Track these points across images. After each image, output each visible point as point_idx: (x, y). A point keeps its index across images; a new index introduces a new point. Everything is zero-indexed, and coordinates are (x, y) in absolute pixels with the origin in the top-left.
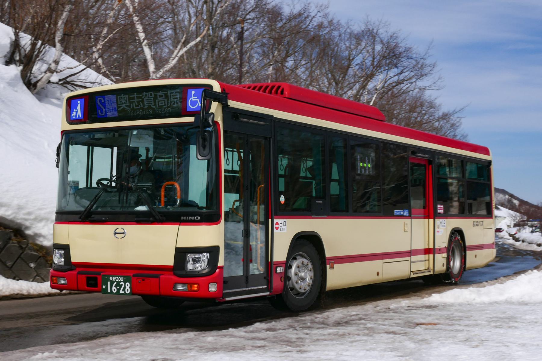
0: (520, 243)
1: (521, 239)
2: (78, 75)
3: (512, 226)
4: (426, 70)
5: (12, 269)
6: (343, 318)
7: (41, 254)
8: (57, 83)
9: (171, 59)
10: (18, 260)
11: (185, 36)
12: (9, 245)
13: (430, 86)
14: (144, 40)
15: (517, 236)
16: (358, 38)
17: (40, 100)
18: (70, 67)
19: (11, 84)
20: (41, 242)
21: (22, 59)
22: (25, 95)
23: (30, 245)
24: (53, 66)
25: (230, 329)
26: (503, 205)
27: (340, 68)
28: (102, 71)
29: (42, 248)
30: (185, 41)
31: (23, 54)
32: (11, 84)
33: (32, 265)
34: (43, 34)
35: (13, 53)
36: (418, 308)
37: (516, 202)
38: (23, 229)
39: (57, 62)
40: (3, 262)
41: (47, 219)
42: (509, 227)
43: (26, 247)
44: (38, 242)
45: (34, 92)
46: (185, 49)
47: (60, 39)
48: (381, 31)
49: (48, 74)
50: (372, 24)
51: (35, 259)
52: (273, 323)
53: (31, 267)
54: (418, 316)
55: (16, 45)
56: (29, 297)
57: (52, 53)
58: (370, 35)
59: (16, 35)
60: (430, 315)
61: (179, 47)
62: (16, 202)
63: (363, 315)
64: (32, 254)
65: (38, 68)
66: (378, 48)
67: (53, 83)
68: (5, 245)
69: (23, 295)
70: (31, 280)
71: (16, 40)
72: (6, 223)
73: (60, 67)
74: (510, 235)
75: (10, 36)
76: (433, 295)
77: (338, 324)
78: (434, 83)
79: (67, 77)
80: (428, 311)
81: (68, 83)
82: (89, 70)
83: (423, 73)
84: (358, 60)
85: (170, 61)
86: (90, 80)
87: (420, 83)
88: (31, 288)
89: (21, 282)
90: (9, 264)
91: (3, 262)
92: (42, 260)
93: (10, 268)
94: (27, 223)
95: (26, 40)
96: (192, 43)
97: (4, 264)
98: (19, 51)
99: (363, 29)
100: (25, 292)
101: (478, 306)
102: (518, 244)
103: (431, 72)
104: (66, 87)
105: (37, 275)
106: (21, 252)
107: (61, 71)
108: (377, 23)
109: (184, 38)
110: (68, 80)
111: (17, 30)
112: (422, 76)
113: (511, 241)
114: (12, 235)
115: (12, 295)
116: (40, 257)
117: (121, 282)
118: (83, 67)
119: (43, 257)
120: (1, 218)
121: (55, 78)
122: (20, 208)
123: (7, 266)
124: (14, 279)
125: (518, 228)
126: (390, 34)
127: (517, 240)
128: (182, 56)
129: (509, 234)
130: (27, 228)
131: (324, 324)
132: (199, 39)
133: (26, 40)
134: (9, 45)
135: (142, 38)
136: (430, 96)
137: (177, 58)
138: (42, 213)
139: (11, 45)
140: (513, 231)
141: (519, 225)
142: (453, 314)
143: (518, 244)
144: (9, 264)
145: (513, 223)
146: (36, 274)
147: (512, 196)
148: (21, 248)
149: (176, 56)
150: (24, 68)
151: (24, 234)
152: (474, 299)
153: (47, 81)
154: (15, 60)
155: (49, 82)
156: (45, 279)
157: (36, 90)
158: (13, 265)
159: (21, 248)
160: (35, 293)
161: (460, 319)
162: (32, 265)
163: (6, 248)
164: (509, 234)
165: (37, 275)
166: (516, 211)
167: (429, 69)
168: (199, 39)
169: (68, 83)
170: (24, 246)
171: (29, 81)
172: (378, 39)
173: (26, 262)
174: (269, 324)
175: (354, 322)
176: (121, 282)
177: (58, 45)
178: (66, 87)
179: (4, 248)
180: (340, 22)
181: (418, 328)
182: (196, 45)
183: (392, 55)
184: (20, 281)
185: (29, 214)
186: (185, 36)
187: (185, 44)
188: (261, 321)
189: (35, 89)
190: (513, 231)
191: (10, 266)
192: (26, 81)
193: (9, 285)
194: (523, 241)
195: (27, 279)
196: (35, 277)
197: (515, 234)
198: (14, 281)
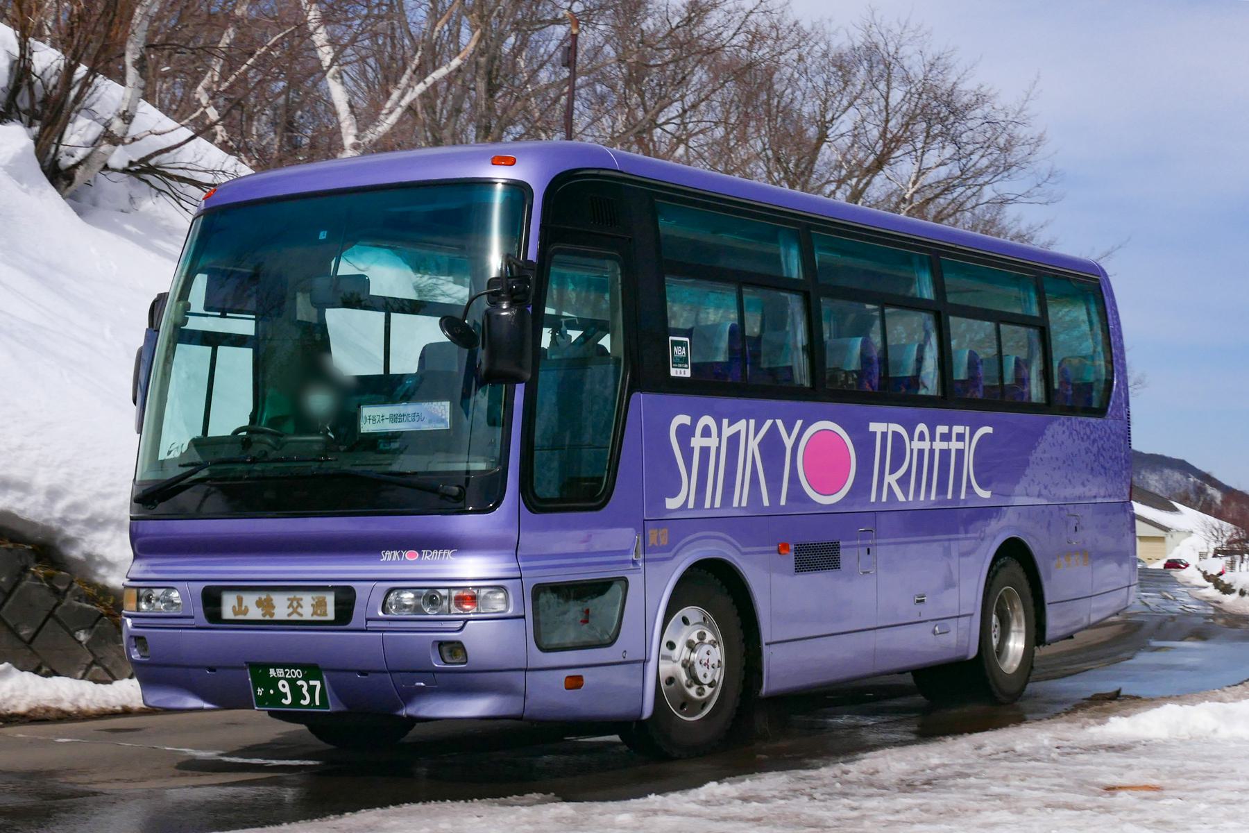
0: (1235, 596)
1: (1237, 587)
2: (175, 151)
3: (1210, 555)
4: (1018, 153)
5: (32, 646)
6: (914, 773)
7: (101, 610)
8: (125, 171)
9: (384, 112)
10: (48, 623)
11: (419, 54)
12: (24, 584)
13: (1028, 194)
14: (330, 67)
15: (1226, 579)
16: (842, 66)
17: (80, 213)
18: (158, 129)
19: (14, 170)
20: (104, 577)
21: (38, 107)
22: (49, 199)
23: (76, 586)
24: (117, 126)
25: (652, 797)
26: (1185, 501)
27: (798, 146)
28: (219, 138)
29: (105, 591)
30: (418, 67)
31: (39, 94)
32: (14, 170)
33: (82, 636)
34: (95, 47)
35: (14, 91)
36: (1095, 748)
37: (1218, 495)
38: (57, 542)
39: (127, 117)
40: (9, 628)
41: (119, 524)
42: (1202, 556)
43: (66, 591)
44: (97, 580)
45: (67, 193)
46: (420, 88)
47: (137, 57)
48: (906, 51)
49: (105, 147)
50: (884, 32)
51: (90, 621)
52: (748, 782)
53: (80, 642)
54: (1107, 770)
55: (21, 70)
56: (63, 717)
57: (110, 95)
58: (877, 62)
59: (23, 45)
60: (1129, 767)
61: (404, 80)
62: (42, 480)
63: (962, 765)
64: (81, 608)
65: (79, 134)
66: (896, 96)
67: (114, 170)
68: (16, 585)
69: (64, 712)
70: (80, 674)
71: (22, 56)
72: (18, 527)
73: (134, 130)
74: (1208, 578)
75: (8, 48)
76: (1112, 719)
77: (907, 786)
78: (1039, 186)
79: (151, 156)
80: (1114, 758)
81: (153, 170)
82: (200, 141)
83: (1009, 160)
84: (844, 124)
85: (382, 117)
86: (204, 164)
87: (1003, 187)
88: (83, 694)
89: (56, 681)
90: (25, 632)
91: (9, 628)
92: (106, 623)
93: (29, 643)
94: (70, 532)
95: (46, 58)
96: (443, 71)
97: (13, 631)
98: (31, 85)
99: (857, 44)
100: (66, 706)
101: (1233, 745)
102: (1230, 600)
103: (1032, 158)
104: (147, 181)
105: (94, 663)
106: (55, 602)
107: (134, 140)
108: (897, 30)
109: (416, 61)
110: (152, 162)
111: (26, 33)
112: (1008, 167)
113: (1211, 592)
114: (31, 559)
115: (35, 710)
116: (102, 615)
117: (297, 679)
118: (187, 133)
119: (108, 615)
120: (6, 515)
121: (119, 157)
122: (53, 494)
123: (20, 638)
124: (37, 671)
125: (1229, 558)
126: (929, 58)
127: (1227, 589)
128: (410, 108)
129: (1205, 573)
130: (70, 542)
131: (874, 785)
132: (456, 62)
133: (46, 58)
134: (6, 71)
135: (327, 61)
136: (1018, 220)
137: (399, 111)
138: (98, 507)
139: (11, 69)
140: (1216, 565)
141: (1229, 551)
142: (1183, 765)
143: (1230, 600)
144: (25, 632)
145: (1213, 546)
146: (91, 659)
147: (1207, 478)
148: (56, 592)
149: (397, 104)
150: (42, 130)
151: (61, 556)
152: (1215, 731)
153: (101, 166)
154: (18, 110)
155: (106, 167)
156: (114, 673)
157: (72, 188)
158: (35, 635)
159: (56, 592)
160: (93, 707)
161: (1210, 776)
162: (82, 636)
163: (17, 591)
164: (1205, 573)
165: (94, 663)
166: (1218, 515)
167: (1027, 149)
168: (456, 62)
169: (153, 170)
170: (61, 588)
171: (55, 162)
172: (897, 72)
173: (66, 629)
174: (739, 785)
175: (951, 782)
176: (297, 679)
177: (132, 74)
178: (147, 181)
179: (11, 591)
180: (801, 23)
181: (1123, 796)
182: (450, 79)
183: (938, 112)
184: (55, 679)
185: (75, 507)
186: (419, 54)
187: (421, 73)
188: (719, 779)
189: (70, 185)
190: (1216, 565)
191: (27, 639)
192: (47, 164)
193: (26, 687)
194: (1242, 593)
195: (71, 675)
196: (89, 666)
197: (1221, 574)
198: (38, 678)
